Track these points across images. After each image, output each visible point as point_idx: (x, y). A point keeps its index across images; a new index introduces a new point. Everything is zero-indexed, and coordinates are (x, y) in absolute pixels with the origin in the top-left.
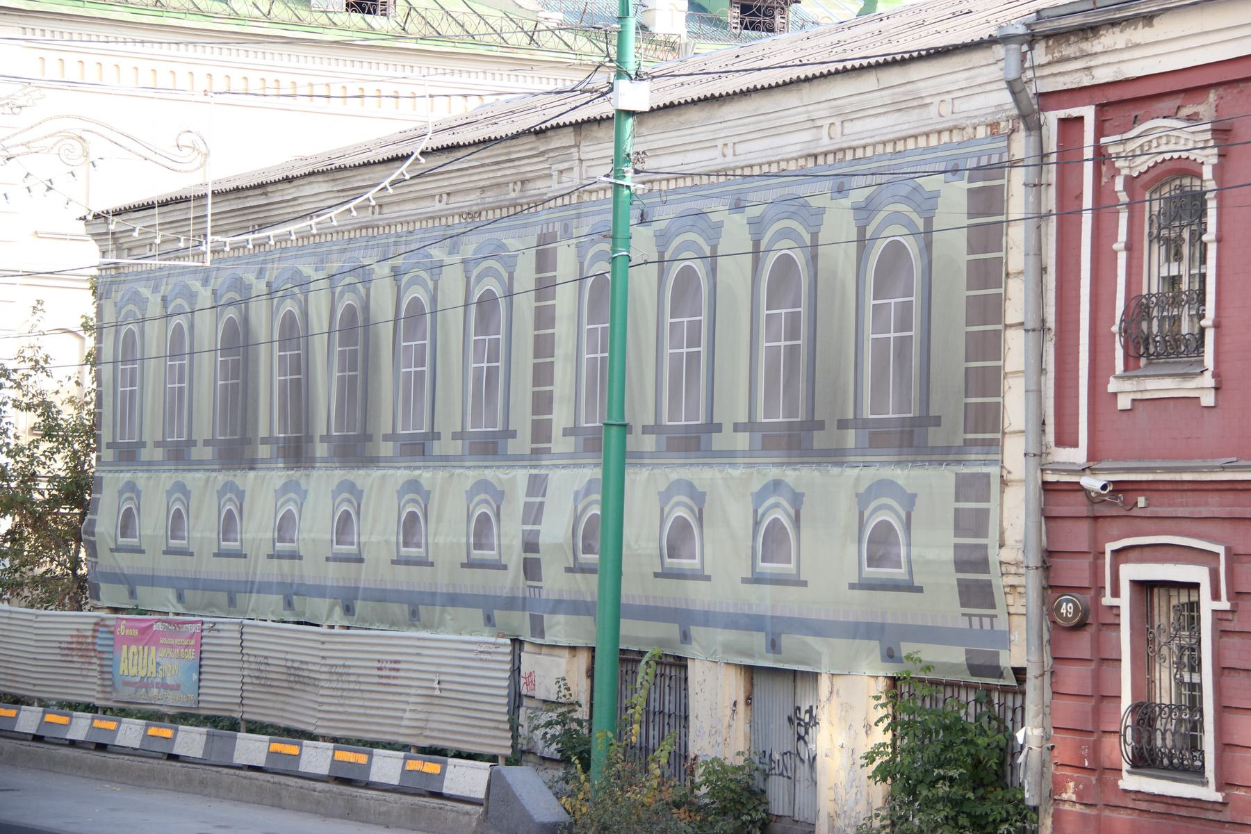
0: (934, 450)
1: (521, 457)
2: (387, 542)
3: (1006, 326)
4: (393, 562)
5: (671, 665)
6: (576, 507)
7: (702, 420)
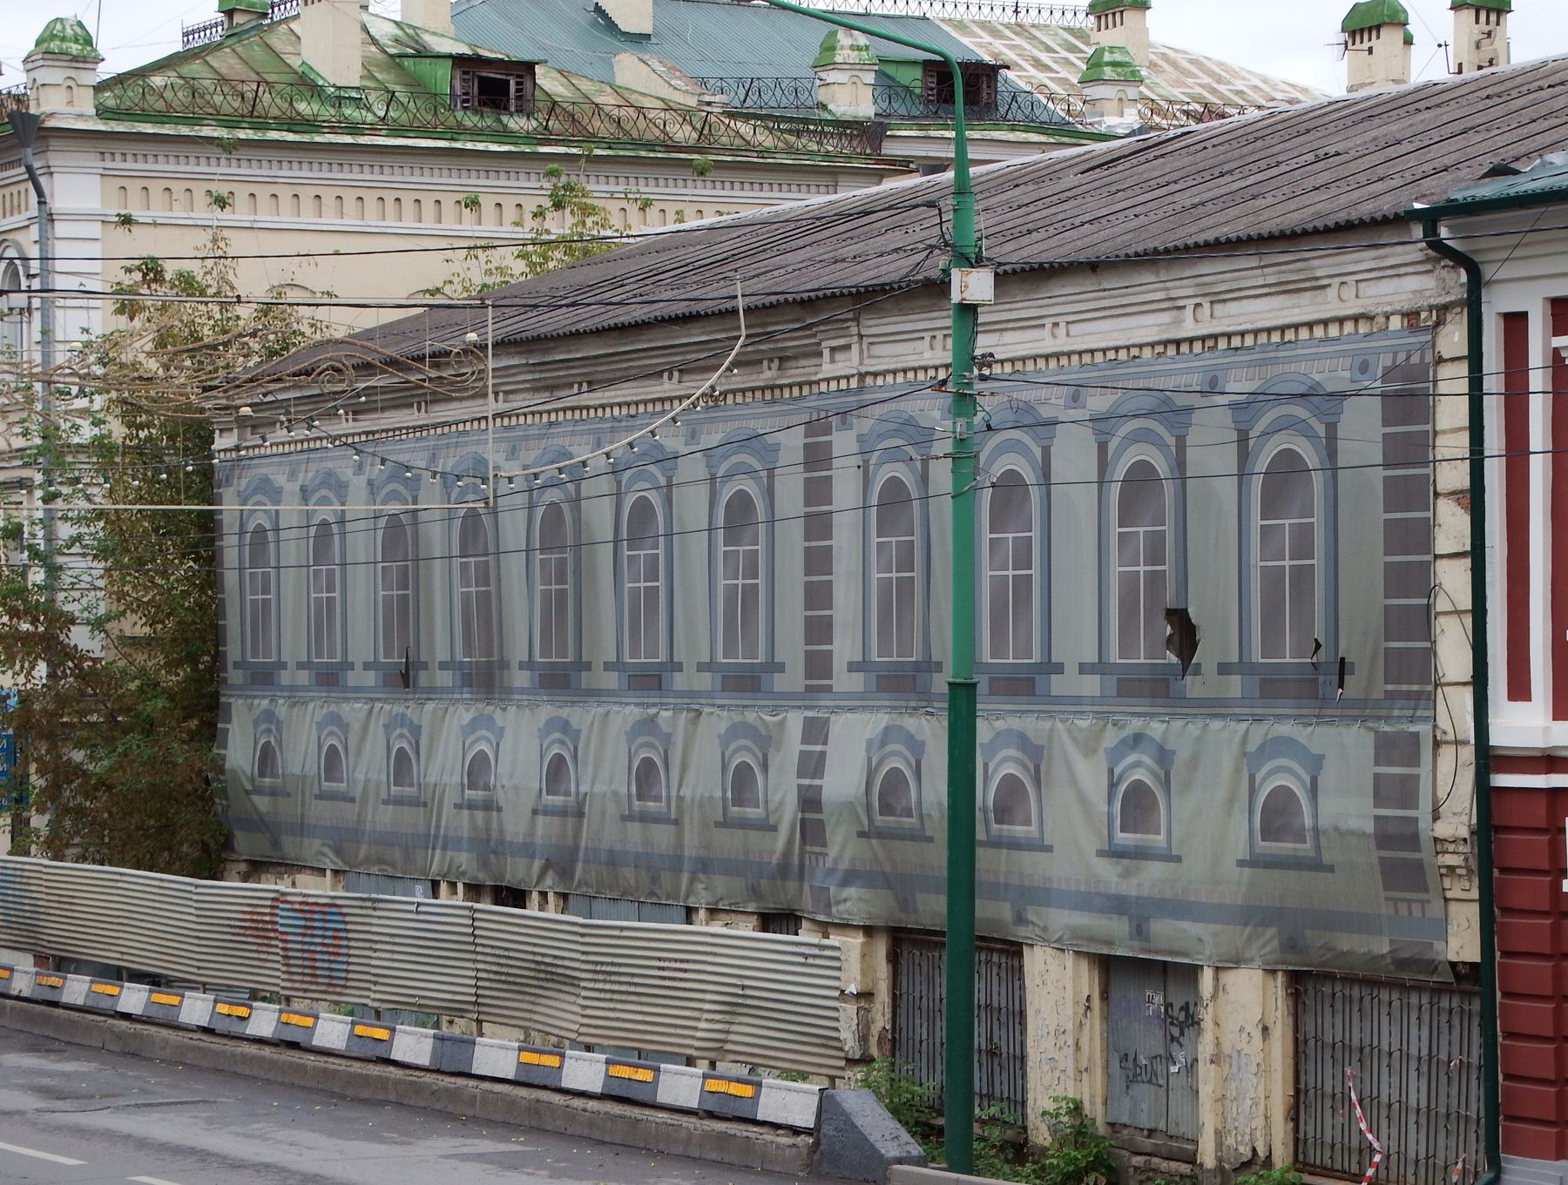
0: (1059, 700)
1: (791, 696)
2: (615, 794)
3: (1436, 557)
4: (624, 818)
5: (1001, 951)
6: (870, 760)
7: (1036, 658)
